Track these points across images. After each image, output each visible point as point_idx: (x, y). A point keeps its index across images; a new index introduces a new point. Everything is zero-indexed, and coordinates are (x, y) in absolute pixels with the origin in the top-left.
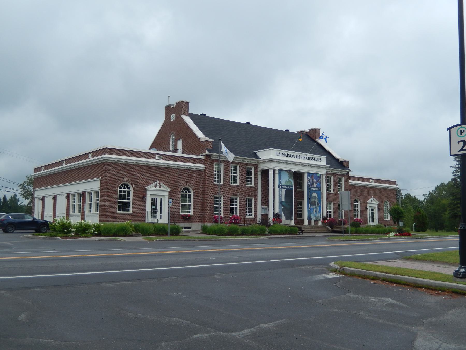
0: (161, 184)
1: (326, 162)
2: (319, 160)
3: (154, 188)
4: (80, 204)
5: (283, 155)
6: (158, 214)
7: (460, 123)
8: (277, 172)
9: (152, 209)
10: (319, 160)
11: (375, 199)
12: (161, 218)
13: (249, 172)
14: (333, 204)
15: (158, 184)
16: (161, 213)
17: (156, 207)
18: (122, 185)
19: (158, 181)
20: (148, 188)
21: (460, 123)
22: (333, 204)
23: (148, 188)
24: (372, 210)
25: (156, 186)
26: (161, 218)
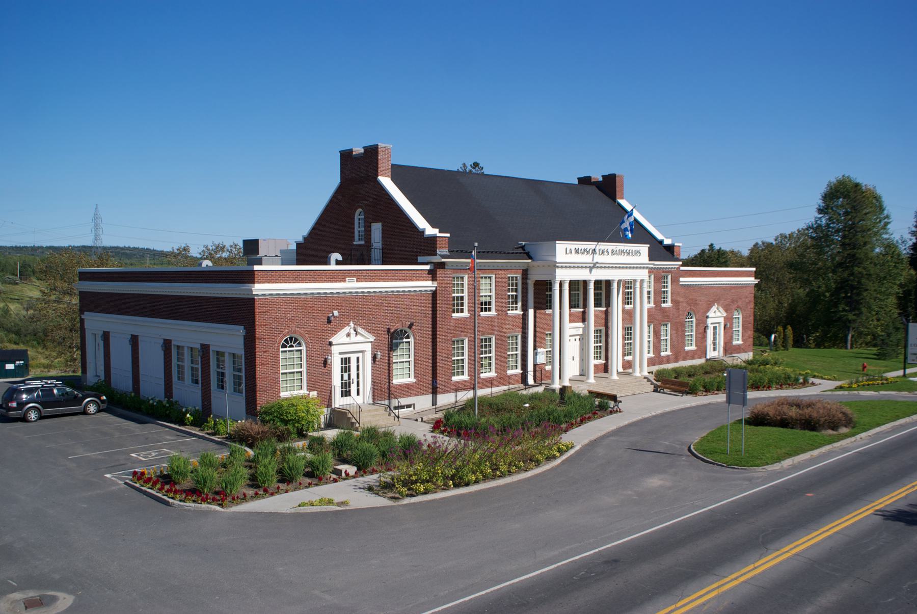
0: (360, 330)
1: (649, 256)
2: (637, 253)
3: (347, 340)
4: (240, 377)
5: (577, 251)
6: (353, 388)
7: (241, 330)
8: (566, 287)
9: (342, 379)
10: (636, 254)
11: (721, 309)
12: (358, 394)
13: (458, 304)
14: (669, 325)
15: (352, 332)
16: (358, 385)
17: (349, 375)
18: (286, 341)
19: (352, 325)
20: (334, 340)
21: (241, 330)
22: (669, 325)
23: (334, 340)
24: (715, 328)
25: (348, 335)
26: (358, 394)
